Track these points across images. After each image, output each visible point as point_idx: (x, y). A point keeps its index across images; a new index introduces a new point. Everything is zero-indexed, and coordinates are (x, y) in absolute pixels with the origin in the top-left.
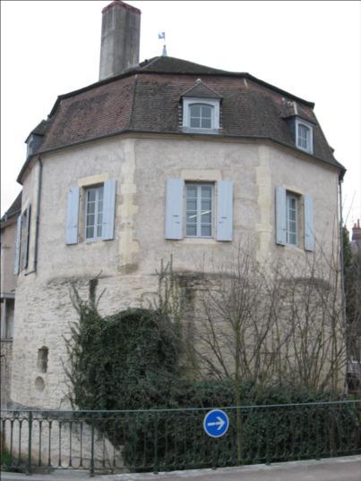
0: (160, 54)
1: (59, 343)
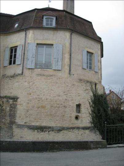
0: (47, 7)
1: (86, 103)
